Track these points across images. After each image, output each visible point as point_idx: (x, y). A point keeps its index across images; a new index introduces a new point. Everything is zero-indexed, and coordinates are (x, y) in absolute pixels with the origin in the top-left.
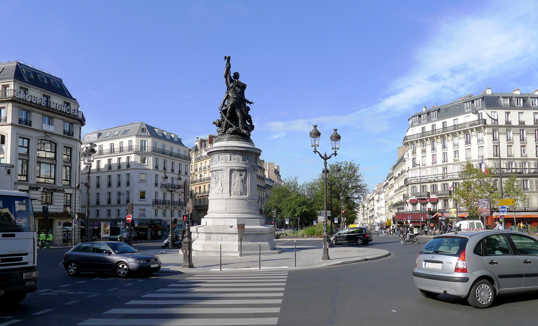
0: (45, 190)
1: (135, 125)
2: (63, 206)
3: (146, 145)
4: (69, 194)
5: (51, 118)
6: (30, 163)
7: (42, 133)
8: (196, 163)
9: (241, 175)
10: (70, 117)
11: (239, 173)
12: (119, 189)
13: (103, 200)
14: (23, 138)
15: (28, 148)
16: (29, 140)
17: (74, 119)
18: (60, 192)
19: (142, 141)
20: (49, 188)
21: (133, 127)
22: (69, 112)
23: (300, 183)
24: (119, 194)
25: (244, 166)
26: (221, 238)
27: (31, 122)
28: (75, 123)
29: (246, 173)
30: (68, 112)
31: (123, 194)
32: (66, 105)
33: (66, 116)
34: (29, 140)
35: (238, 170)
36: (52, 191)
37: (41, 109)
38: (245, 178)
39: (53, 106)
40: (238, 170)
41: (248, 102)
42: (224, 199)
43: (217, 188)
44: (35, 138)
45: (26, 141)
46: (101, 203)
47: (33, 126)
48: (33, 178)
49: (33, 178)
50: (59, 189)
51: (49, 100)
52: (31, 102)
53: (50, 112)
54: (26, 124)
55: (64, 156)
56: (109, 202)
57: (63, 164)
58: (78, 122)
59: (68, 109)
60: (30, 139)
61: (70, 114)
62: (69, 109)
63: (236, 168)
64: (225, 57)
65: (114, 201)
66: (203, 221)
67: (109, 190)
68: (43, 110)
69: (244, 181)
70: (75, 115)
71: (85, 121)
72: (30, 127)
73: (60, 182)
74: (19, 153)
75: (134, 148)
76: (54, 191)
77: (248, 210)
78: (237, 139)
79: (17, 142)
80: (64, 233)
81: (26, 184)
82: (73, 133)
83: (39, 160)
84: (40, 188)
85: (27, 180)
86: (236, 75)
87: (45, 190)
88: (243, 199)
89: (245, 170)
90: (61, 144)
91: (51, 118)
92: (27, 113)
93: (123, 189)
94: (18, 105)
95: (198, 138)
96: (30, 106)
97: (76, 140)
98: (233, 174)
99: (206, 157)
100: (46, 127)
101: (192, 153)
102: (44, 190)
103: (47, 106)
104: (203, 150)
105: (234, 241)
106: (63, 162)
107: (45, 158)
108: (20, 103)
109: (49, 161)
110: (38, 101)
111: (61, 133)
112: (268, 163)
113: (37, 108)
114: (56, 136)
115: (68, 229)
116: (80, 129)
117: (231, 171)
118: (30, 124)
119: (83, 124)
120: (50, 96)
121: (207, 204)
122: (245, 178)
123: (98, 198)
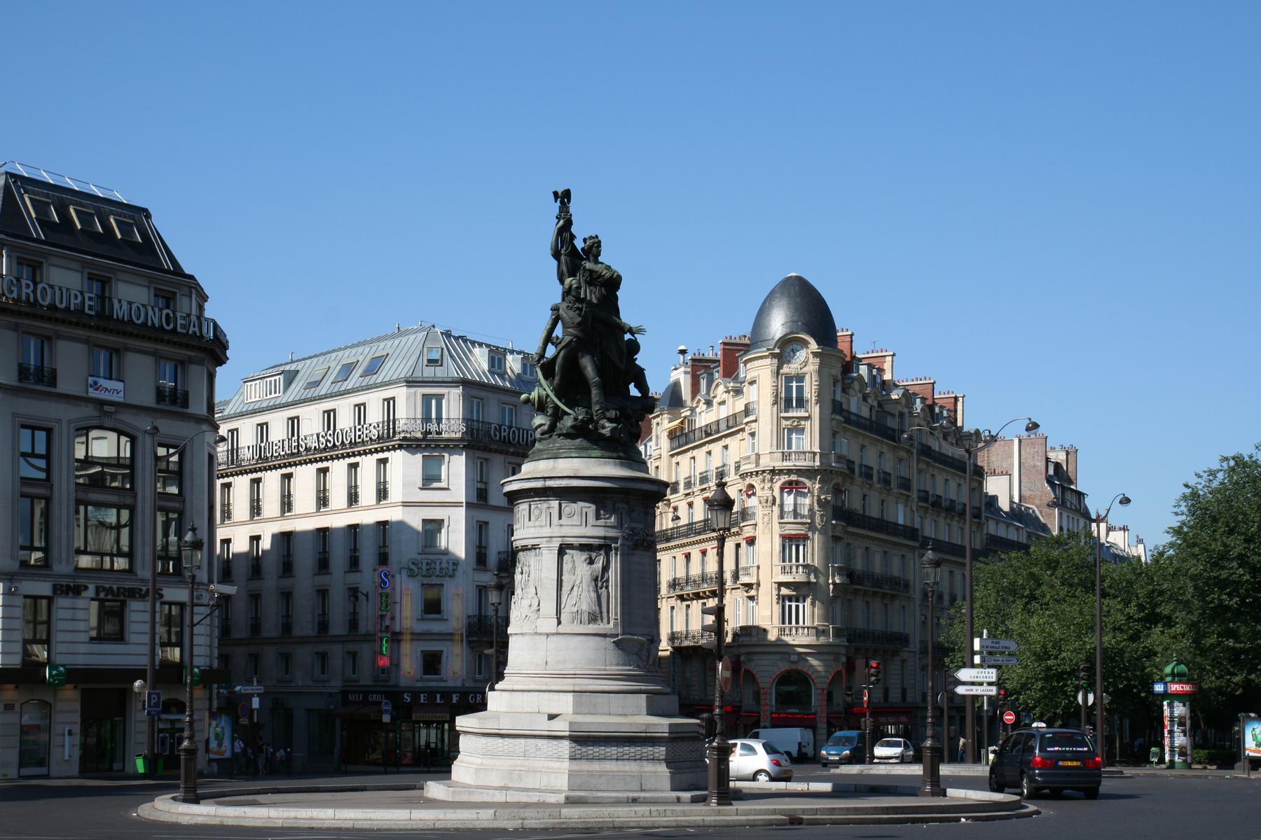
1: (414, 336)
3: (444, 416)
4: (176, 603)
5: (115, 352)
6: (55, 508)
7: (91, 406)
8: (675, 460)
9: (591, 562)
10: (175, 343)
11: (585, 556)
12: (353, 578)
13: (304, 624)
14: (34, 428)
15: (47, 457)
16: (49, 432)
17: (187, 346)
19: (427, 399)
20: (115, 587)
21: (401, 346)
24: (354, 592)
25: (601, 532)
26: (525, 751)
27: (54, 373)
28: (191, 361)
29: (607, 556)
30: (168, 324)
31: (367, 595)
32: (161, 302)
33: (162, 341)
34: (49, 432)
35: (583, 548)
36: (122, 598)
37: (84, 326)
38: (605, 568)
39: (120, 311)
40: (583, 548)
41: (631, 331)
42: (540, 634)
43: (526, 602)
45: (41, 436)
46: (297, 632)
47: (63, 386)
48: (64, 556)
49: (64, 556)
51: (107, 294)
52: (53, 307)
53: (111, 331)
54: (40, 381)
56: (323, 626)
58: (203, 355)
59: (168, 315)
60: (52, 429)
61: (174, 330)
62: (172, 315)
63: (576, 542)
64: (555, 194)
66: (493, 698)
67: (322, 580)
68: (91, 327)
69: (599, 581)
70: (190, 332)
71: (224, 347)
72: (52, 390)
74: (22, 478)
75: (401, 425)
76: (129, 597)
77: (614, 669)
78: (582, 453)
79: (15, 441)
80: (161, 735)
81: (45, 577)
83: (82, 496)
84: (86, 588)
85: (46, 564)
86: (594, 248)
88: (604, 636)
89: (604, 547)
92: (43, 342)
93: (367, 577)
94: (14, 320)
95: (683, 352)
96: (49, 319)
97: (198, 420)
98: (566, 558)
99: (711, 434)
101: (658, 416)
102: (97, 593)
103: (101, 315)
104: (701, 404)
105: (559, 758)
108: (20, 314)
110: (73, 301)
111: (149, 400)
112: (1016, 441)
113: (70, 323)
115: (172, 722)
116: (211, 377)
117: (562, 551)
119: (221, 360)
120: (110, 278)
122: (605, 568)
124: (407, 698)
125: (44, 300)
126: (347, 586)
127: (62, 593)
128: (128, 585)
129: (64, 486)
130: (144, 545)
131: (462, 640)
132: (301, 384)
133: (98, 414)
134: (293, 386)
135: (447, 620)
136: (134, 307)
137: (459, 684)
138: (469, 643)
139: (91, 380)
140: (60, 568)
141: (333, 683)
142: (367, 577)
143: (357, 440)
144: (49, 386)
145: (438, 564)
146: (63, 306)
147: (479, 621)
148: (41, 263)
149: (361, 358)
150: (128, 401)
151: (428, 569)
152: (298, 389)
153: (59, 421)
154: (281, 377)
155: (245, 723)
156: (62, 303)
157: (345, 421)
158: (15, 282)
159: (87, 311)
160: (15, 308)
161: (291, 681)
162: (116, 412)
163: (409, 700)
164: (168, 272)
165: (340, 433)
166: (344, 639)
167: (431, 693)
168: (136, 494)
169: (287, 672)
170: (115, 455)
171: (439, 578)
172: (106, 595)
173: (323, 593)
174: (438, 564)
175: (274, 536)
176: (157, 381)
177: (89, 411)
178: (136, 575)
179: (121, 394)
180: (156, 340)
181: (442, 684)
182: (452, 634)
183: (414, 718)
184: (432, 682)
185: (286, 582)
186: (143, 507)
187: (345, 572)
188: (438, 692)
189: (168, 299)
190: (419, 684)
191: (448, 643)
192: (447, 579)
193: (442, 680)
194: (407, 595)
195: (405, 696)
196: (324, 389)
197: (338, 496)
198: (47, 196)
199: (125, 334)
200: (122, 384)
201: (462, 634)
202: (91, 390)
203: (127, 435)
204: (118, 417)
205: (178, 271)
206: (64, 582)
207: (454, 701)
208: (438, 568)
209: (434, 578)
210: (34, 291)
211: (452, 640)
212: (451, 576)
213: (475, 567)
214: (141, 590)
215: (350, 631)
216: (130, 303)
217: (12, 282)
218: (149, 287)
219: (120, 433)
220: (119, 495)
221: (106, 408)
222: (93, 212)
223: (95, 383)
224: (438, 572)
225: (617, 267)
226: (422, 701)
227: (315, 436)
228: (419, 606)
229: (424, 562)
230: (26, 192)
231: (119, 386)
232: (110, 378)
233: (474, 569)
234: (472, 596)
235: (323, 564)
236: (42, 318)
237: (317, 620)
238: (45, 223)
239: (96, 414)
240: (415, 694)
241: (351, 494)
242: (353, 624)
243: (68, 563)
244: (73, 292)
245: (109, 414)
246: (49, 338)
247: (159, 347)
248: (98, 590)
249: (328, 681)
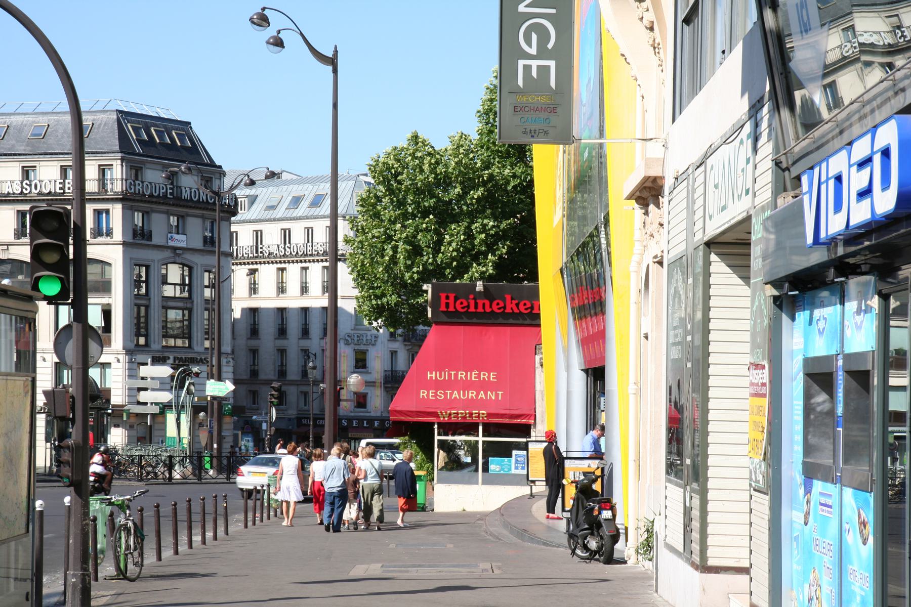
0: (177, 362)
7: (169, 250)
12: (305, 343)
18: (201, 364)
20: (183, 357)
22: (213, 200)
23: (441, 142)
24: (306, 353)
31: (315, 355)
44: (158, 261)
47: (157, 240)
48: (157, 339)
49: (157, 339)
50: (199, 357)
52: (151, 195)
55: (205, 289)
57: (204, 306)
65: (293, 373)
67: (281, 343)
68: (170, 204)
73: (199, 344)
76: (191, 362)
83: (165, 304)
84: (169, 358)
87: (177, 362)
90: (199, 267)
91: (181, 217)
93: (315, 343)
96: (149, 202)
102: (175, 361)
106: (203, 302)
107: (175, 298)
108: (134, 200)
109: (180, 304)
110: (161, 191)
114: (191, 252)
118: (149, 236)
121: (826, 303)
123: (282, 363)
124: (345, 423)
125: (147, 192)
126: (300, 348)
127: (157, 361)
128: (190, 356)
129: (156, 299)
130: (197, 332)
131: (381, 386)
132: (261, 205)
134: (255, 206)
135: (370, 373)
136: (193, 190)
137: (379, 414)
138: (385, 388)
139: (169, 235)
140: (155, 346)
141: (290, 412)
142: (315, 343)
143: (308, 253)
144: (148, 241)
145: (365, 337)
146: (156, 194)
147: (392, 373)
148: (142, 168)
149: (306, 193)
150: (189, 247)
151: (358, 340)
152: (259, 209)
153: (153, 261)
154: (246, 200)
155: (171, 430)
156: (156, 192)
157: (298, 238)
158: (133, 183)
159: (169, 196)
160: (132, 198)
161: (258, 409)
162: (183, 253)
163: (346, 424)
164: (207, 165)
165: (295, 246)
166: (299, 383)
167: (360, 420)
168: (193, 301)
169: (254, 403)
170: (121, 246)
171: (366, 346)
172: (179, 362)
173: (282, 352)
174: (365, 337)
175: (243, 310)
176: (204, 233)
177: (168, 254)
178: (194, 350)
179: (185, 243)
180: (204, 209)
181: (368, 414)
182: (374, 382)
183: (350, 436)
184: (361, 413)
185: (253, 343)
186: (197, 309)
187: (299, 339)
188: (365, 420)
189: (207, 182)
190: (352, 414)
191: (372, 388)
192: (371, 346)
193: (367, 412)
194: (344, 356)
195: (343, 421)
196: (280, 212)
197: (293, 287)
198: (138, 123)
199: (187, 207)
200: (185, 236)
201: (381, 383)
202: (169, 241)
203: (187, 266)
204: (184, 256)
205: (212, 164)
206: (157, 355)
207: (376, 425)
208: (365, 339)
209: (362, 346)
210: (142, 187)
211: (374, 386)
212: (373, 345)
213: (389, 339)
214: (197, 358)
215: (302, 378)
216: (191, 189)
217: (131, 183)
218: (198, 176)
219: (184, 265)
220: (184, 303)
221: (178, 251)
222: (163, 130)
223: (172, 237)
224: (365, 342)
225: (484, 91)
226: (354, 425)
227: (276, 247)
228: (353, 363)
229: (356, 336)
230: (128, 122)
231: (183, 237)
232: (178, 233)
233: (388, 340)
234: (388, 356)
235: (282, 332)
236: (145, 202)
237: (277, 369)
238: (141, 142)
239: (172, 255)
240: (350, 420)
241: (303, 287)
242: (305, 373)
243: (158, 343)
244: (161, 186)
245: (178, 255)
246: (147, 213)
247: (205, 212)
248: (175, 359)
249: (286, 410)
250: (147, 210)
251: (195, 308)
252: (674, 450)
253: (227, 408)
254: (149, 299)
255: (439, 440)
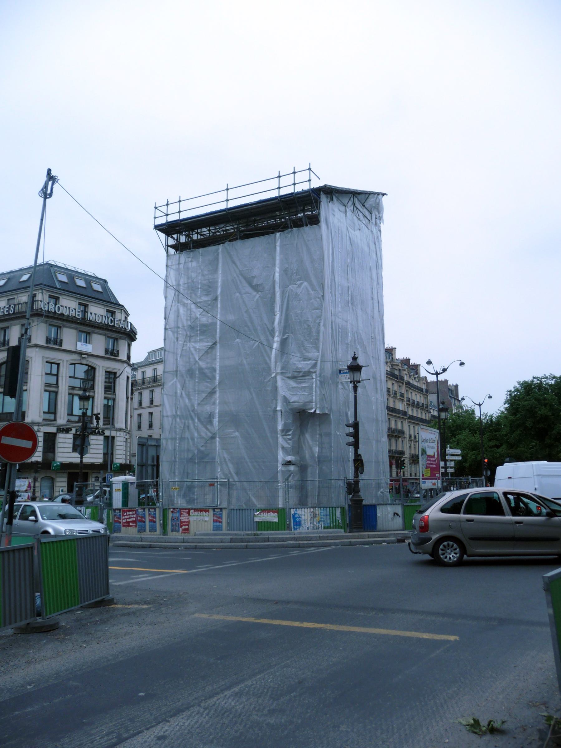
2: (102, 454)
82: (118, 351)
83: (71, 391)
90: (101, 369)
100: (82, 347)
114: (95, 357)
133: (79, 358)
153: (63, 360)
162: (87, 357)
216: (96, 314)
221: (83, 356)
239: (79, 358)
250: (60, 325)
251: (96, 396)
252: (152, 452)
253: (55, 465)
254: (58, 387)
255: (451, 477)
